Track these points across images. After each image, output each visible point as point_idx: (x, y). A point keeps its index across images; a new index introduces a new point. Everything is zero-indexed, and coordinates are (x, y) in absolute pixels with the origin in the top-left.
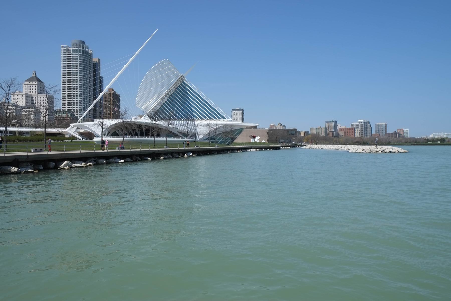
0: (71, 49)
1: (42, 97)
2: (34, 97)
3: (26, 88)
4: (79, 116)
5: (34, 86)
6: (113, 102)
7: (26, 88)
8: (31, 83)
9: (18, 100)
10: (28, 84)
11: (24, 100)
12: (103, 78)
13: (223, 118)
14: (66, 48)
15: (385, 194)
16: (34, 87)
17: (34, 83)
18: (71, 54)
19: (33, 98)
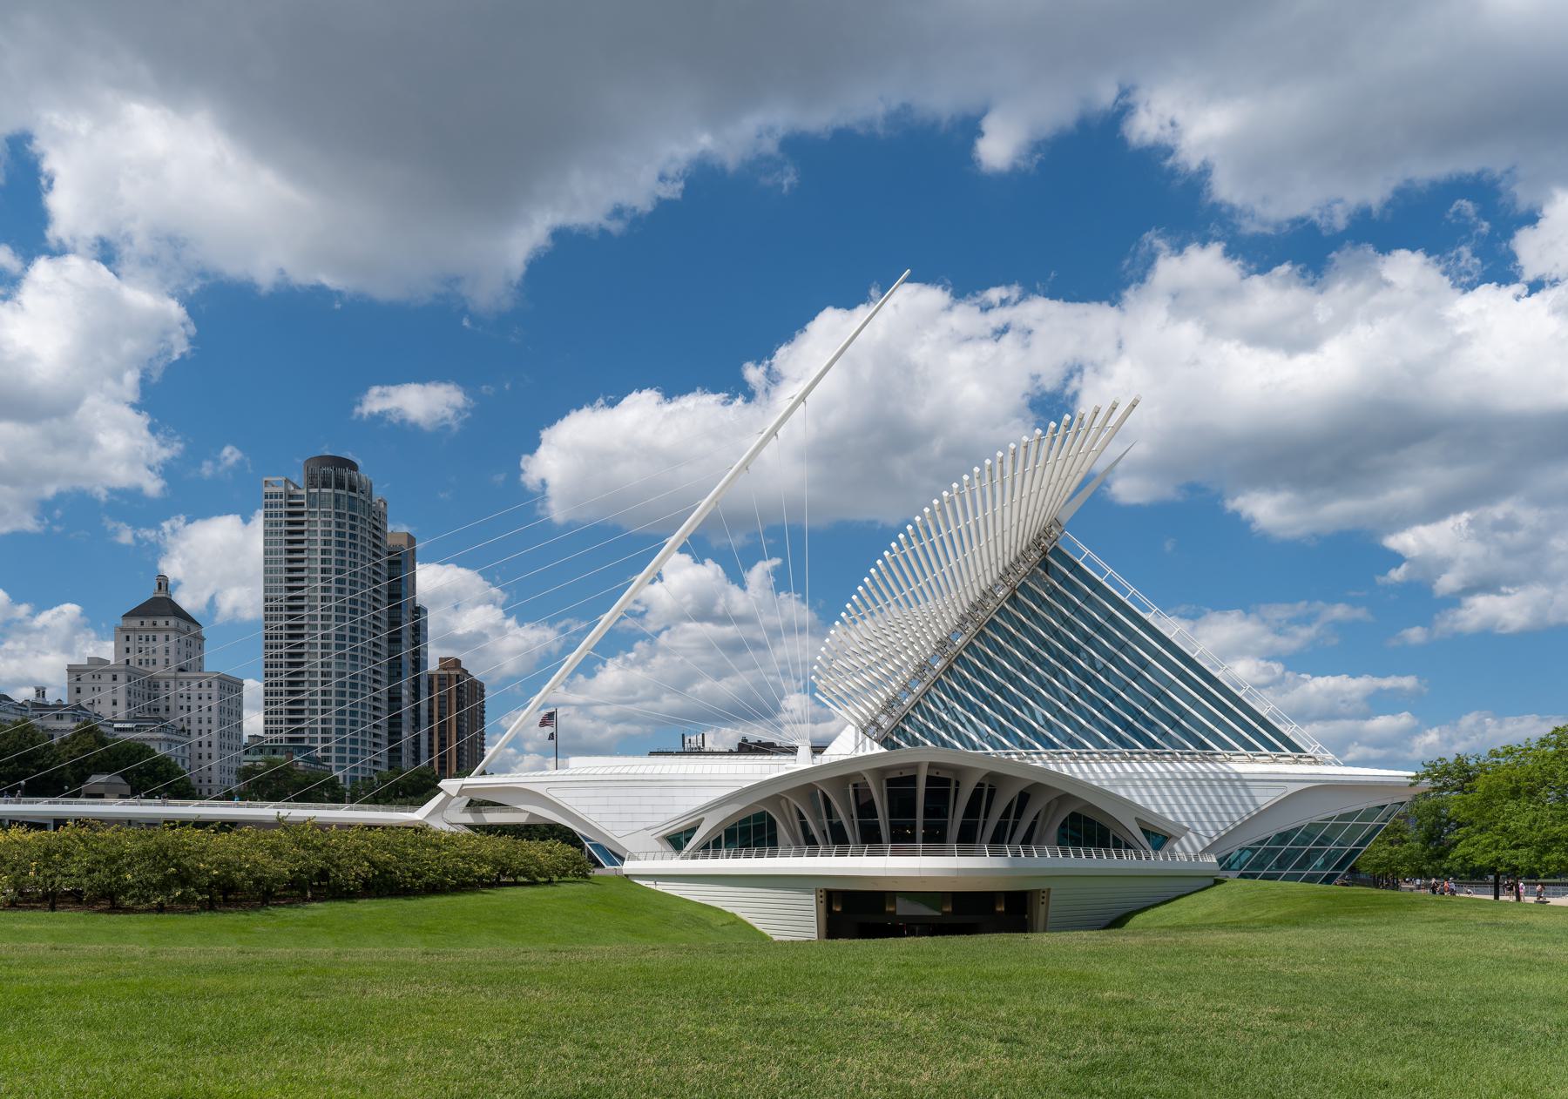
0: (303, 492)
1: (194, 684)
2: (162, 684)
3: (130, 645)
4: (333, 764)
5: (161, 636)
6: (1297, 867)
7: (130, 645)
8: (148, 622)
9: (97, 696)
10: (134, 630)
11: (122, 699)
12: (426, 611)
13: (1294, 747)
14: (281, 489)
15: (1196, 939)
16: (160, 645)
17: (161, 622)
18: (302, 514)
19: (157, 686)
